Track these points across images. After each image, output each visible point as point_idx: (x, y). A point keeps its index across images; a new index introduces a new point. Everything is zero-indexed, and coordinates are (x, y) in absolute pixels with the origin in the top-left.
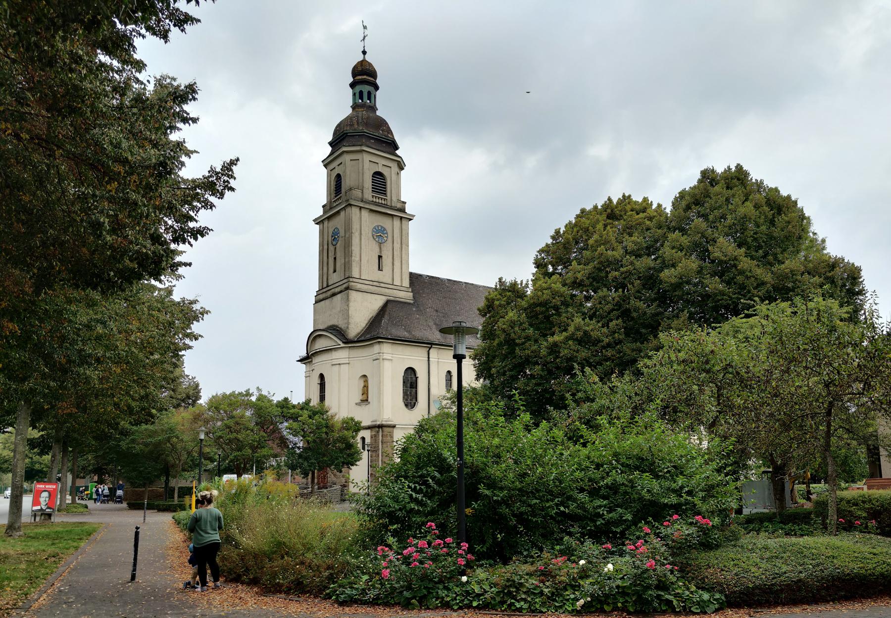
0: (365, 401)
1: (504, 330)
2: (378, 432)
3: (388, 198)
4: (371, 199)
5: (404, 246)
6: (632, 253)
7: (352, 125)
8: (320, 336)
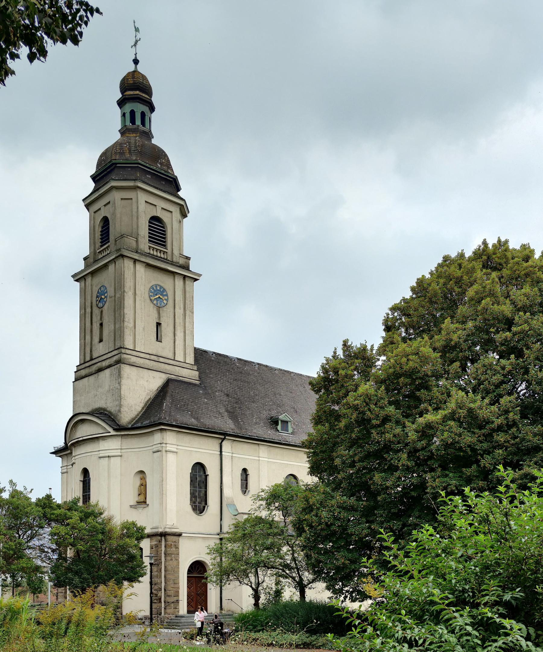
0: (142, 503)
1: (356, 408)
2: (160, 541)
3: (169, 251)
4: (147, 251)
5: (188, 312)
6: (524, 309)
7: (122, 154)
8: (83, 421)
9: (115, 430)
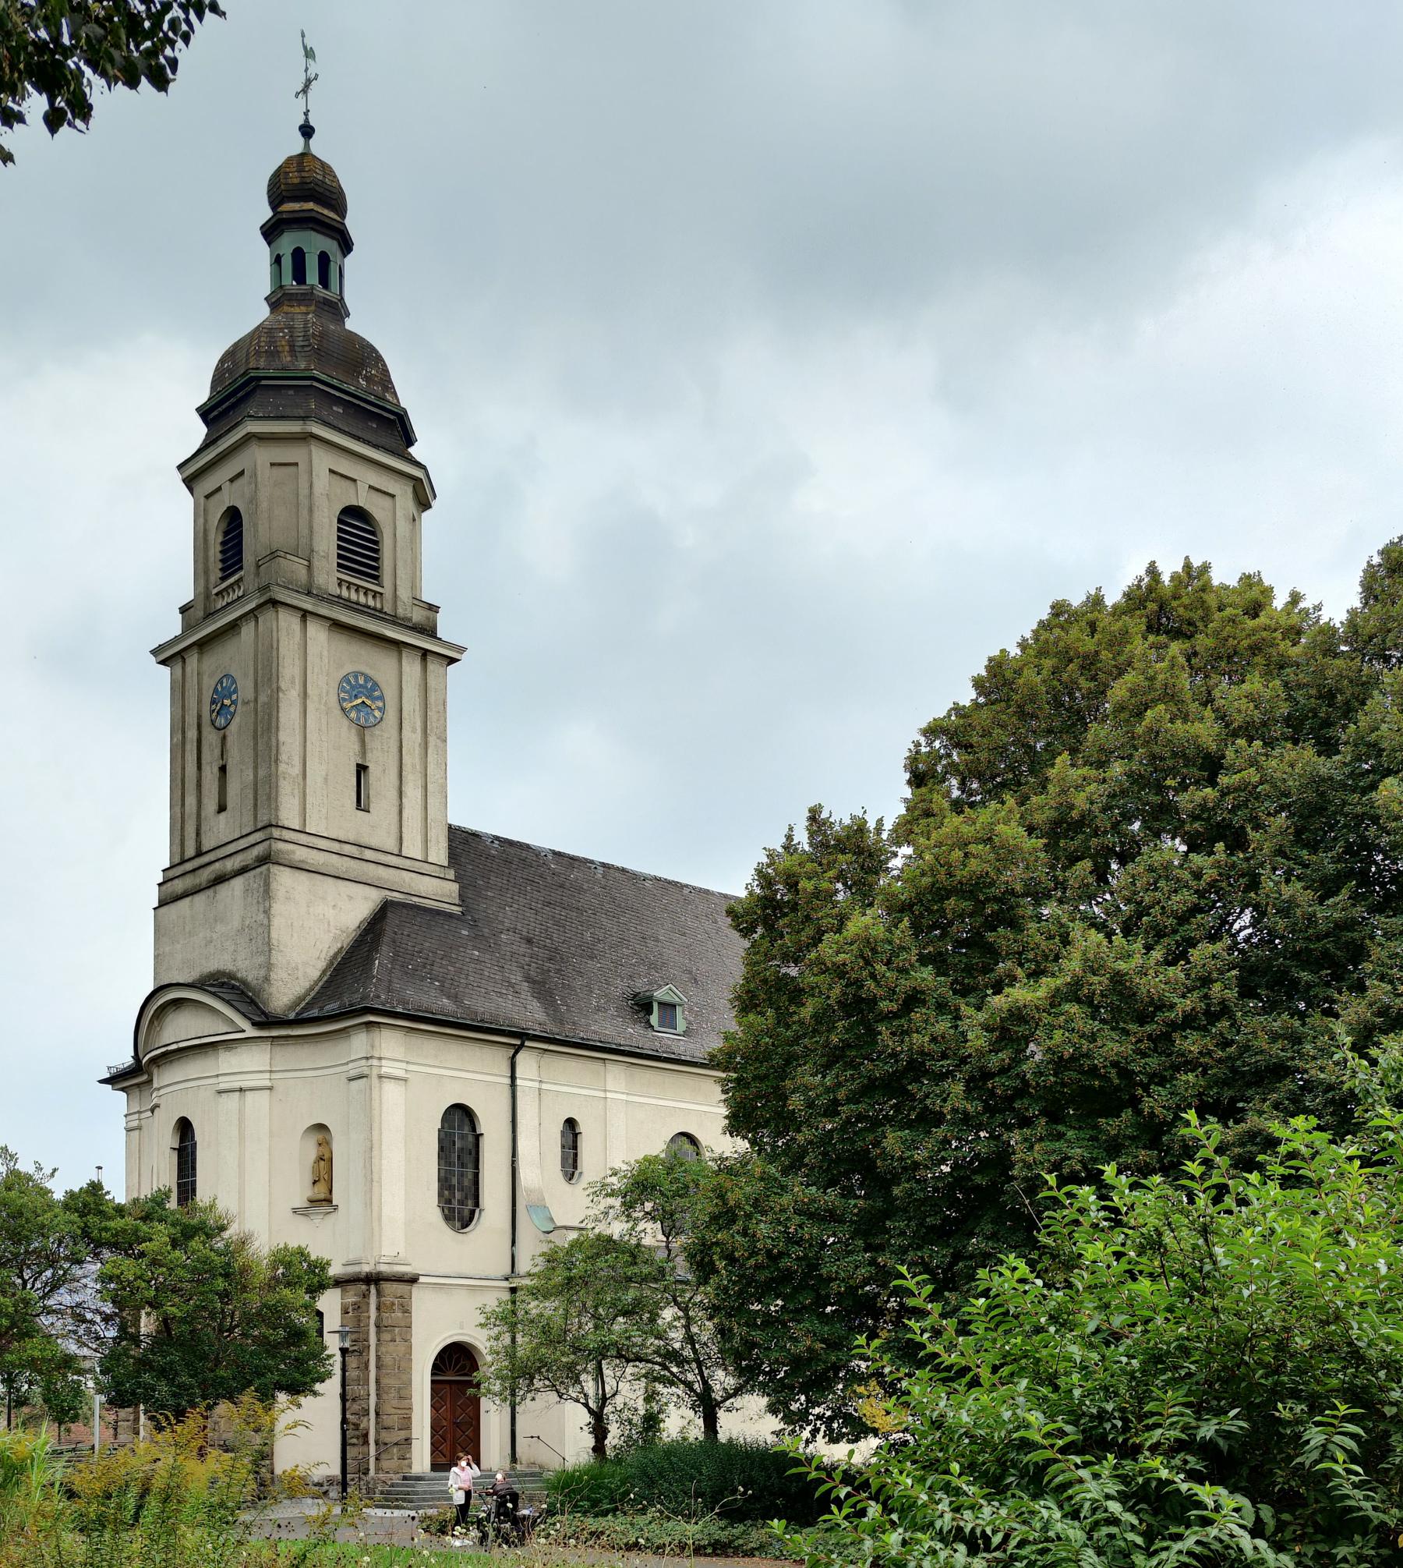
0: (322, 1201)
1: (840, 971)
3: (387, 590)
4: (334, 589)
5: (432, 740)
6: (1248, 731)
7: (273, 354)
8: (177, 1003)
9: (256, 1025)
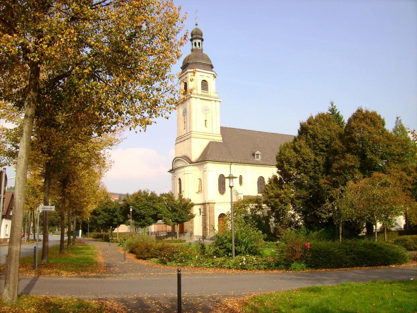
4: (201, 93)
9: (190, 163)
